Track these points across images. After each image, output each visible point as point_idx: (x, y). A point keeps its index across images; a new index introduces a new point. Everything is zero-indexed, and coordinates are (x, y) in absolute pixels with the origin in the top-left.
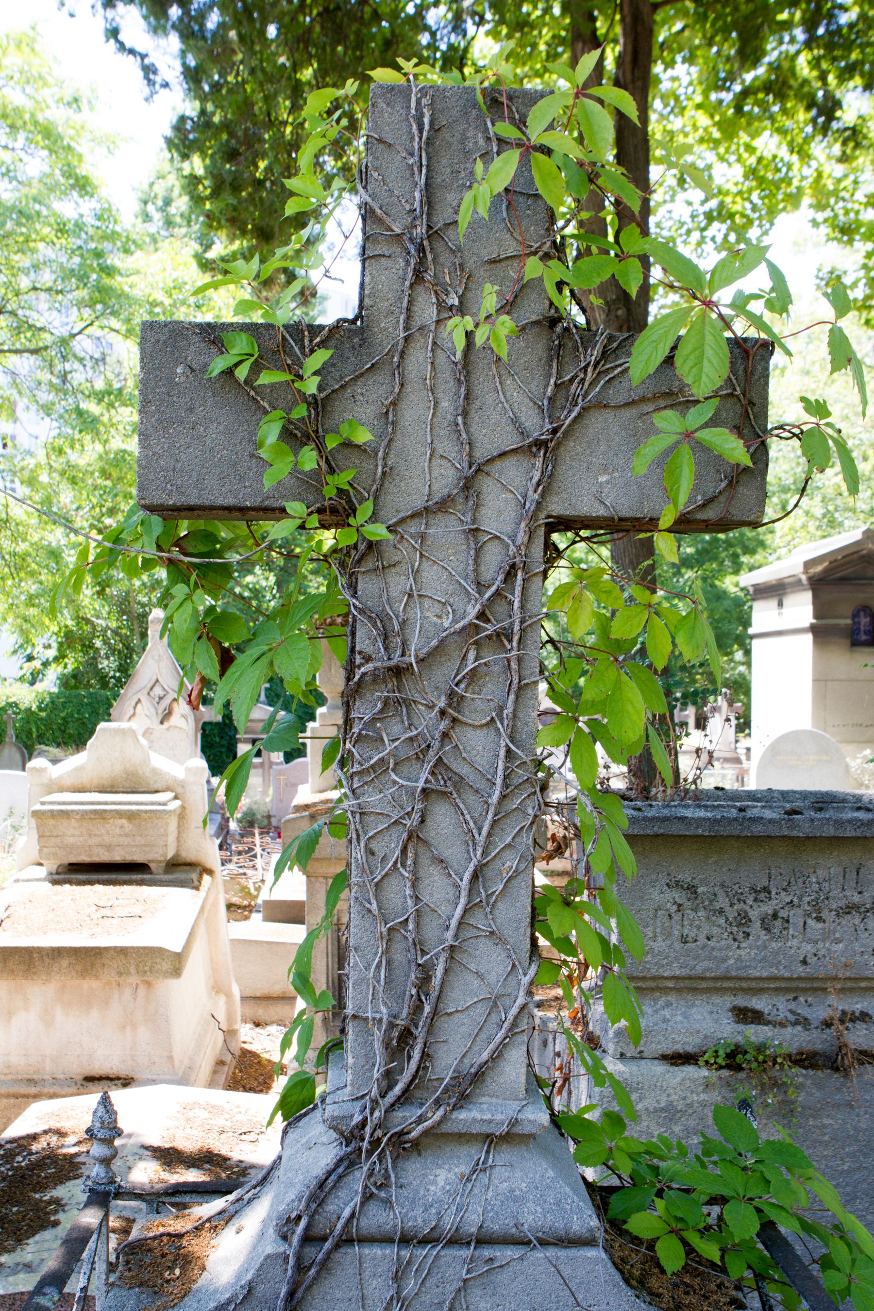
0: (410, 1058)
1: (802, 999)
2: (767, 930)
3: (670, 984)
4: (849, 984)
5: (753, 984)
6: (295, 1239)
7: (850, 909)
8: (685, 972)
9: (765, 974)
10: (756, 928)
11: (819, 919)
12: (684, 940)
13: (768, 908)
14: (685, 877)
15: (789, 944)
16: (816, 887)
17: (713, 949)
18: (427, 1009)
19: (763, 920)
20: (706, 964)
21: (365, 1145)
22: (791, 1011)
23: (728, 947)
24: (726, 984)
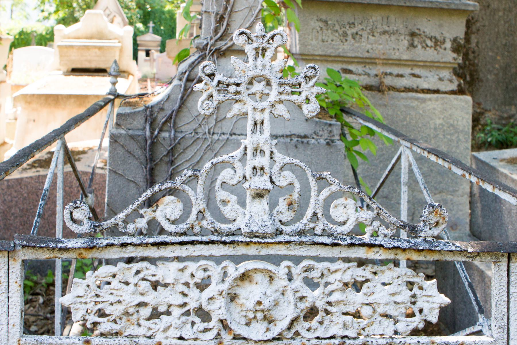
0: (223, 25)
1: (367, 67)
2: (354, 39)
3: (318, 58)
4: (385, 61)
5: (349, 60)
6: (184, 80)
7: (385, 32)
8: (323, 53)
9: (353, 55)
10: (350, 38)
11: (373, 36)
12: (323, 41)
13: (354, 31)
14: (324, 17)
15: (362, 44)
16: (372, 24)
17: (334, 45)
18: (229, 9)
19: (352, 35)
20: (331, 50)
21: (207, 52)
22: (364, 71)
23: (339, 44)
24: (339, 59)
